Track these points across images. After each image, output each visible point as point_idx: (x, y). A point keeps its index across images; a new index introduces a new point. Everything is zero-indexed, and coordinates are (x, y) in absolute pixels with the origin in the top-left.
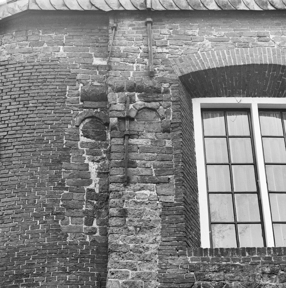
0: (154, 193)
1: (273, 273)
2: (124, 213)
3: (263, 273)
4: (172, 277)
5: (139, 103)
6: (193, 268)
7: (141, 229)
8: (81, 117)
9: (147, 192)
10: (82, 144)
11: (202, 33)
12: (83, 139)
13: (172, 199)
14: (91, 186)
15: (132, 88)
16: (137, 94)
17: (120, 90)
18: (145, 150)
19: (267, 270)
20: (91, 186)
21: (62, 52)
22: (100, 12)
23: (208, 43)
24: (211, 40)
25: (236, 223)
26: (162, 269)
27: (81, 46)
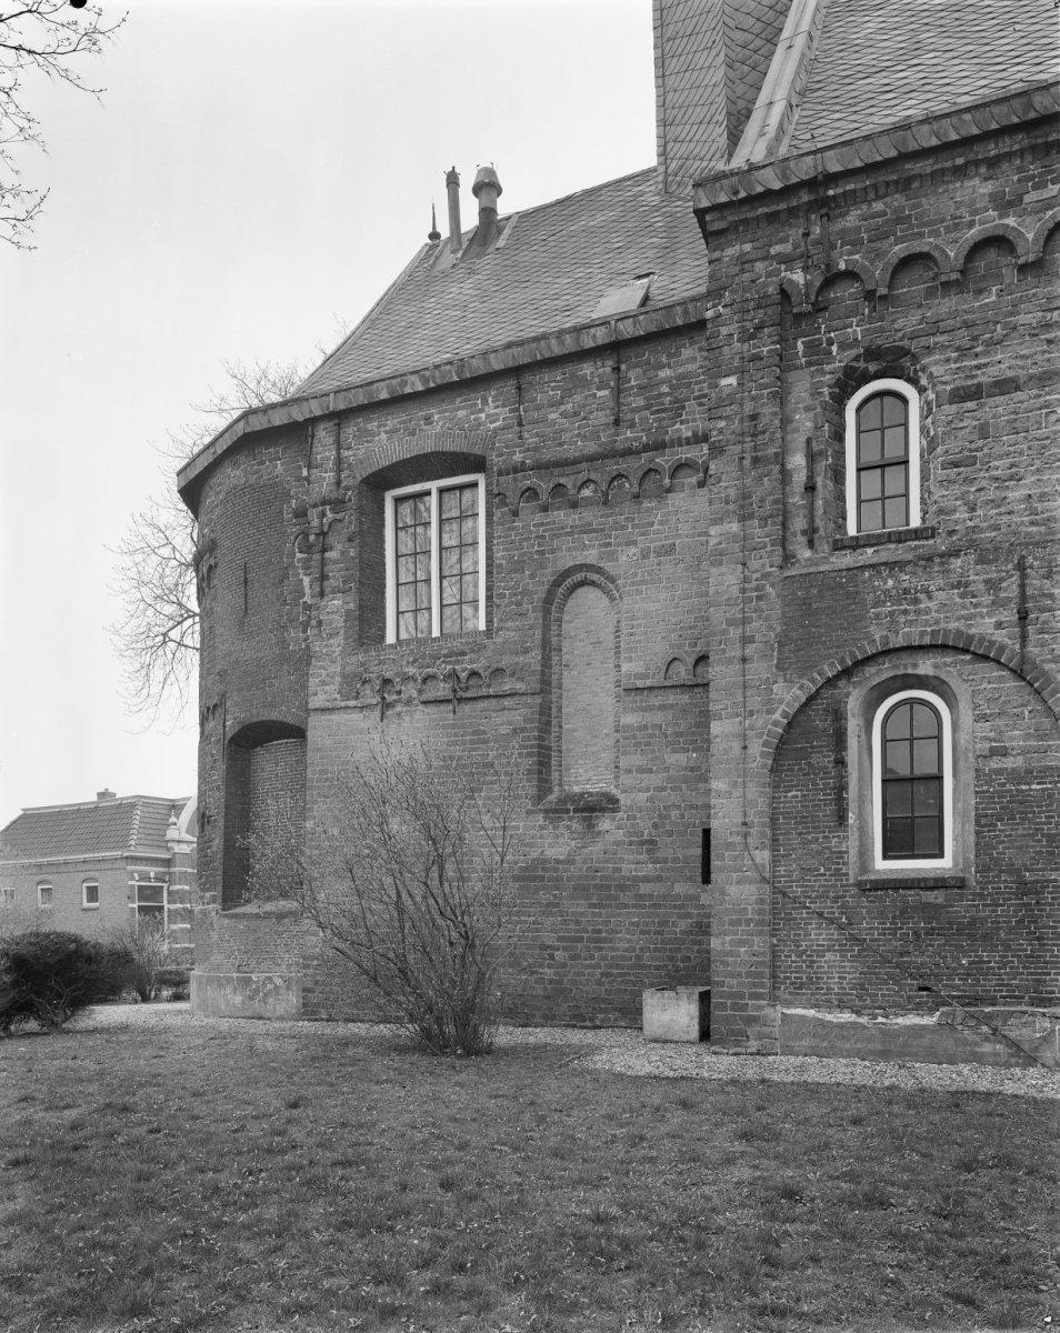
0: (340, 602)
1: (415, 661)
2: (320, 623)
3: (408, 662)
4: (761, 847)
5: (330, 515)
6: (362, 664)
7: (331, 636)
8: (295, 535)
9: (335, 602)
10: (299, 560)
11: (379, 426)
12: (299, 555)
13: (352, 606)
14: (305, 599)
15: (324, 503)
16: (328, 507)
17: (315, 506)
18: (336, 562)
19: (411, 659)
20: (305, 599)
21: (668, 373)
22: (296, 423)
23: (384, 436)
24: (386, 432)
25: (912, 740)
26: (343, 667)
27: (339, 449)
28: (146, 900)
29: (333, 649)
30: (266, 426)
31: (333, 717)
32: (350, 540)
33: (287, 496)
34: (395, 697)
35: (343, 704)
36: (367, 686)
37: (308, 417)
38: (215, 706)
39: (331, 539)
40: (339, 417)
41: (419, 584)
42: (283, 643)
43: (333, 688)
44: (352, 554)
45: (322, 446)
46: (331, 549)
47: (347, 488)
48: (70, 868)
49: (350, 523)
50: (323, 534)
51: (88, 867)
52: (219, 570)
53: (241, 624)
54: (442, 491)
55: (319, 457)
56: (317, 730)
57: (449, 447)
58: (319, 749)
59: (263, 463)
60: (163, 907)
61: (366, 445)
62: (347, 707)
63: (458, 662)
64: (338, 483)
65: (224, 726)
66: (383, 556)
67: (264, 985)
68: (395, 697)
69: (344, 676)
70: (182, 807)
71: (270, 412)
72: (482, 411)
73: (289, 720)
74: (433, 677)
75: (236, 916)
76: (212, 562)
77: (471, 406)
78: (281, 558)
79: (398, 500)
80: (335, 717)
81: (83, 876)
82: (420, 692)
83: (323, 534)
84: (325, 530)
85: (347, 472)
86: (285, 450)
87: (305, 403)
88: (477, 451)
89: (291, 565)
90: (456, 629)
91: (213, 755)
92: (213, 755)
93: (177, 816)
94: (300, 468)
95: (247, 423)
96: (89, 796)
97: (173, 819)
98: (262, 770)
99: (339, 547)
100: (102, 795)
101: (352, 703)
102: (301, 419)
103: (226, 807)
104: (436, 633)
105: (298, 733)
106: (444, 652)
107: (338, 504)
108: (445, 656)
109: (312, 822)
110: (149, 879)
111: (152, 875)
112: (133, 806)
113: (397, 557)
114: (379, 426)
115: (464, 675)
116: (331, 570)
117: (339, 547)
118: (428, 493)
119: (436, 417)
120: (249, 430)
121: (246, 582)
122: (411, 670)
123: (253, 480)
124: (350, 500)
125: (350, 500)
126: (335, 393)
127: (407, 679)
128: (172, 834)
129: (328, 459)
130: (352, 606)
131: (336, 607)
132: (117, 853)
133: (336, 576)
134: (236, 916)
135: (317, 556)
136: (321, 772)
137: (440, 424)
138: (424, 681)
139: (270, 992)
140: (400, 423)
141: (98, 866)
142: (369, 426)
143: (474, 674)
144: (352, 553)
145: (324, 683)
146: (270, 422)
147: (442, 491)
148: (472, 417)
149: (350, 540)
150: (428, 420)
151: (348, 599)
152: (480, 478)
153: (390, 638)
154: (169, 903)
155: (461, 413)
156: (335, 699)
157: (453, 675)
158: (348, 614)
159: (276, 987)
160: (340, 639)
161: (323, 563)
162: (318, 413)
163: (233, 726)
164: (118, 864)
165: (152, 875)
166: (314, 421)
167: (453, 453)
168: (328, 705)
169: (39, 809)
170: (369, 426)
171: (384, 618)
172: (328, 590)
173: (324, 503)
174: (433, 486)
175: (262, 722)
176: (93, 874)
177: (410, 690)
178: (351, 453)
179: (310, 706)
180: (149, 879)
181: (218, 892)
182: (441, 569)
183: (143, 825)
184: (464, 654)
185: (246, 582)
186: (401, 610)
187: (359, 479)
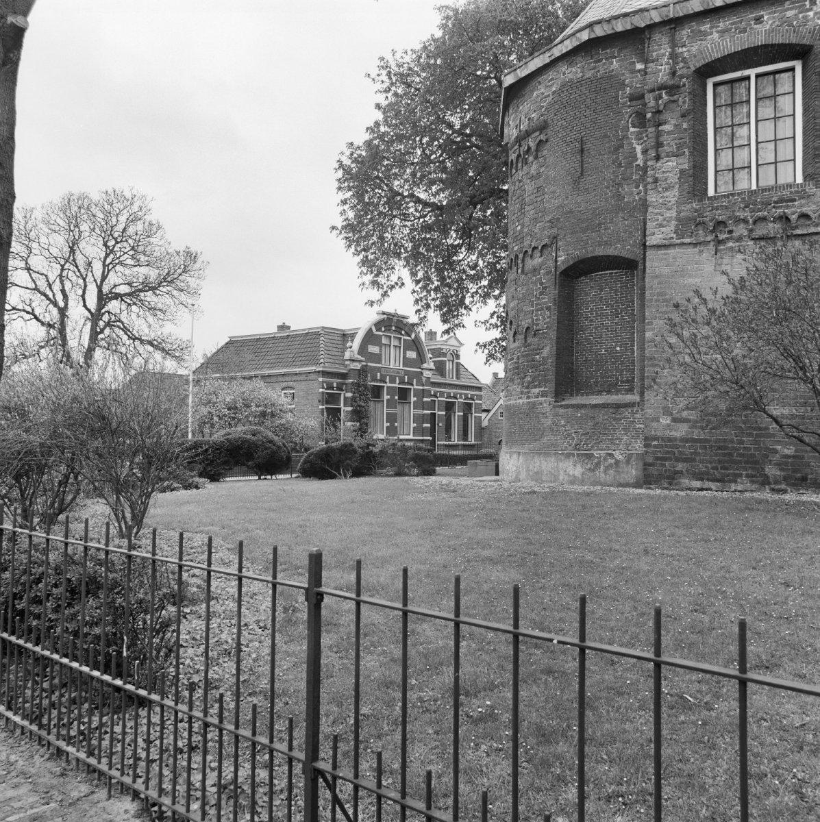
0: (675, 164)
1: (746, 207)
2: (656, 180)
6: (696, 211)
7: (667, 189)
12: (632, 130)
13: (686, 166)
14: (637, 163)
15: (660, 89)
16: (664, 92)
17: (652, 91)
18: (669, 133)
19: (742, 206)
20: (637, 163)
23: (716, 35)
24: (718, 32)
26: (679, 213)
28: (330, 404)
29: (669, 199)
30: (610, 32)
31: (669, 251)
32: (683, 116)
33: (623, 85)
34: (727, 236)
35: (679, 241)
36: (700, 227)
37: (648, 23)
38: (544, 246)
39: (666, 116)
40: (674, 23)
41: (735, 149)
42: (619, 197)
43: (670, 230)
44: (684, 127)
45: (658, 45)
46: (665, 123)
47: (682, 77)
48: (273, 379)
49: (684, 102)
50: (658, 112)
51: (287, 378)
52: (548, 146)
53: (576, 182)
54: (758, 76)
55: (654, 54)
56: (655, 264)
57: (778, 40)
58: (657, 277)
59: (600, 61)
60: (339, 410)
61: (699, 43)
62: (683, 244)
63: (787, 207)
64: (673, 74)
65: (556, 261)
66: (706, 129)
67: (605, 459)
68: (727, 236)
69: (678, 219)
70: (353, 336)
71: (614, 22)
72: (811, 10)
73: (624, 254)
74: (764, 219)
75: (567, 406)
76: (543, 137)
77: (800, 7)
78: (617, 132)
79: (716, 85)
80: (671, 251)
81: (283, 385)
82: (751, 231)
83: (658, 112)
84: (661, 108)
85: (681, 65)
86: (620, 50)
87: (646, 14)
88: (806, 41)
89: (625, 137)
90: (772, 182)
91: (542, 283)
92: (542, 283)
93: (352, 341)
94: (634, 63)
95: (593, 31)
96: (270, 329)
97: (349, 344)
98: (586, 294)
99: (673, 122)
100: (283, 327)
101: (687, 240)
102: (643, 25)
103: (558, 322)
104: (754, 187)
105: (630, 266)
106: (775, 199)
107: (672, 89)
108: (775, 202)
109: (651, 333)
110: (332, 388)
111: (335, 385)
112: (317, 334)
113: (794, 115)
114: (711, 28)
115: (794, 217)
116: (665, 139)
117: (673, 122)
118: (748, 78)
119: (765, 18)
120: (593, 36)
121: (582, 151)
122: (742, 215)
123: (589, 74)
124: (684, 85)
125: (684, 85)
126: (674, 4)
127: (738, 221)
128: (347, 355)
129: (663, 55)
130: (686, 166)
131: (671, 167)
132: (313, 368)
133: (669, 143)
134: (567, 406)
135: (651, 130)
136: (659, 294)
137: (770, 22)
138: (755, 222)
139: (610, 465)
140: (732, 24)
141: (294, 378)
142: (702, 28)
143: (805, 216)
144: (685, 125)
145: (661, 226)
146: (613, 29)
147: (758, 76)
148: (801, 16)
149: (683, 116)
150: (758, 20)
151: (681, 161)
152: (798, 65)
153: (711, 192)
154: (345, 406)
155: (790, 13)
156: (672, 238)
157: (785, 219)
158: (682, 172)
159: (617, 462)
160: (676, 192)
161: (659, 134)
162: (657, 19)
163: (563, 262)
164: (313, 376)
165: (335, 385)
166: (651, 27)
167: (779, 45)
168: (667, 242)
169: (242, 337)
170: (702, 28)
171: (707, 176)
172: (663, 155)
173: (660, 89)
174: (752, 72)
175: (597, 257)
176: (290, 384)
177: (741, 230)
178: (685, 49)
179: (647, 244)
180: (332, 388)
181: (551, 387)
182: (757, 136)
183: (326, 348)
184: (794, 200)
185: (582, 151)
186: (760, 163)
187: (693, 69)
